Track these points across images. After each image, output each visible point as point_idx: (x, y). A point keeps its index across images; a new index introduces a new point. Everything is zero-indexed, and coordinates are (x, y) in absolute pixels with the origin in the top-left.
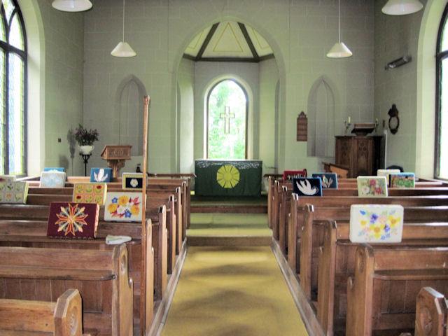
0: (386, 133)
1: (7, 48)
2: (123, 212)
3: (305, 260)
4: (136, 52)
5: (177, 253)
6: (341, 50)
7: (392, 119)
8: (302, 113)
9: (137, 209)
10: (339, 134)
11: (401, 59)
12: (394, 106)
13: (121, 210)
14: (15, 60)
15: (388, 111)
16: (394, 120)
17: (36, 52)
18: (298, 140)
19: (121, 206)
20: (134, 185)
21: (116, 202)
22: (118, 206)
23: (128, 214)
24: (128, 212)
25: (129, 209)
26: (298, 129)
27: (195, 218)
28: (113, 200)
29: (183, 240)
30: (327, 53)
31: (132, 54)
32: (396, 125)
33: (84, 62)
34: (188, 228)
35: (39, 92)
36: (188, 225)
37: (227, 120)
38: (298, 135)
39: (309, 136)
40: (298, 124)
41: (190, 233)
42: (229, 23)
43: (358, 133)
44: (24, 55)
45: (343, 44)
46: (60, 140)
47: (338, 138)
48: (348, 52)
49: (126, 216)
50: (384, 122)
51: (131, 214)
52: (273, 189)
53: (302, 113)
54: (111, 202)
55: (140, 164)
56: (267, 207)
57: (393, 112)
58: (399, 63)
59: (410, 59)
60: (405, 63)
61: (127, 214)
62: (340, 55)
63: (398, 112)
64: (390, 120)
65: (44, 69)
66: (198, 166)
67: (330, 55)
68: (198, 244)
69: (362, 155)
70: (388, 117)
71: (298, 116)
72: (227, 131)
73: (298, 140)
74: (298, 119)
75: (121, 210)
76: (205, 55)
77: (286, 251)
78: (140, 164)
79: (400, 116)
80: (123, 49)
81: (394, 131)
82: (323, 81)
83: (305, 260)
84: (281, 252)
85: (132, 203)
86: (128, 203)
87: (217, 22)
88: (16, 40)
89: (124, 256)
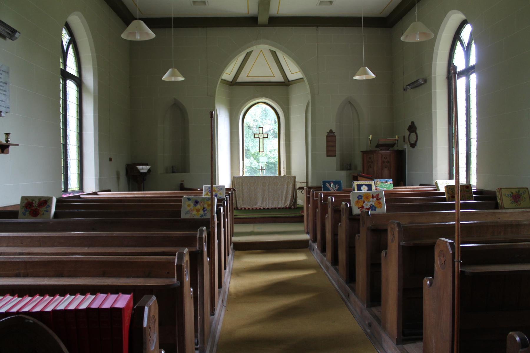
0: (407, 147)
1: (66, 76)
2: (368, 206)
3: (342, 256)
4: (185, 78)
5: (228, 255)
6: (366, 73)
7: (412, 134)
8: (331, 131)
9: (380, 203)
10: (365, 149)
11: (417, 81)
12: (413, 123)
13: (367, 205)
14: (71, 87)
15: (407, 127)
16: (413, 136)
17: (89, 79)
18: (328, 156)
19: (366, 202)
20: (364, 186)
21: (361, 199)
22: (364, 202)
23: (373, 208)
24: (373, 206)
25: (373, 204)
26: (328, 146)
27: (238, 228)
28: (358, 197)
29: (231, 245)
30: (353, 77)
31: (182, 79)
32: (415, 139)
33: (130, 87)
34: (233, 236)
35: (93, 114)
36: (233, 234)
37: (261, 140)
38: (328, 151)
39: (338, 152)
40: (328, 141)
41: (235, 239)
42: (261, 51)
43: (381, 148)
44: (79, 82)
45: (367, 68)
46: (111, 160)
47: (363, 152)
48: (372, 75)
49: (372, 210)
50: (404, 137)
51: (375, 208)
52: (308, 199)
53: (331, 131)
54: (357, 199)
55: (183, 181)
56: (303, 216)
57: (412, 128)
58: (415, 85)
59: (425, 81)
60: (421, 84)
61: (372, 208)
62: (364, 77)
63: (416, 128)
64: (409, 135)
65: (97, 94)
66: (235, 180)
67: (356, 78)
68: (241, 247)
69: (386, 167)
70: (408, 133)
71: (327, 134)
72: (261, 150)
73: (328, 156)
74: (327, 136)
75: (367, 205)
76: (239, 80)
77: (323, 249)
78: (183, 181)
79: (418, 132)
80: (173, 75)
81: (413, 145)
82: (350, 103)
83: (342, 256)
84: (319, 252)
85: (375, 199)
86: (371, 199)
87: (252, 50)
88: (72, 68)
89: (187, 261)
